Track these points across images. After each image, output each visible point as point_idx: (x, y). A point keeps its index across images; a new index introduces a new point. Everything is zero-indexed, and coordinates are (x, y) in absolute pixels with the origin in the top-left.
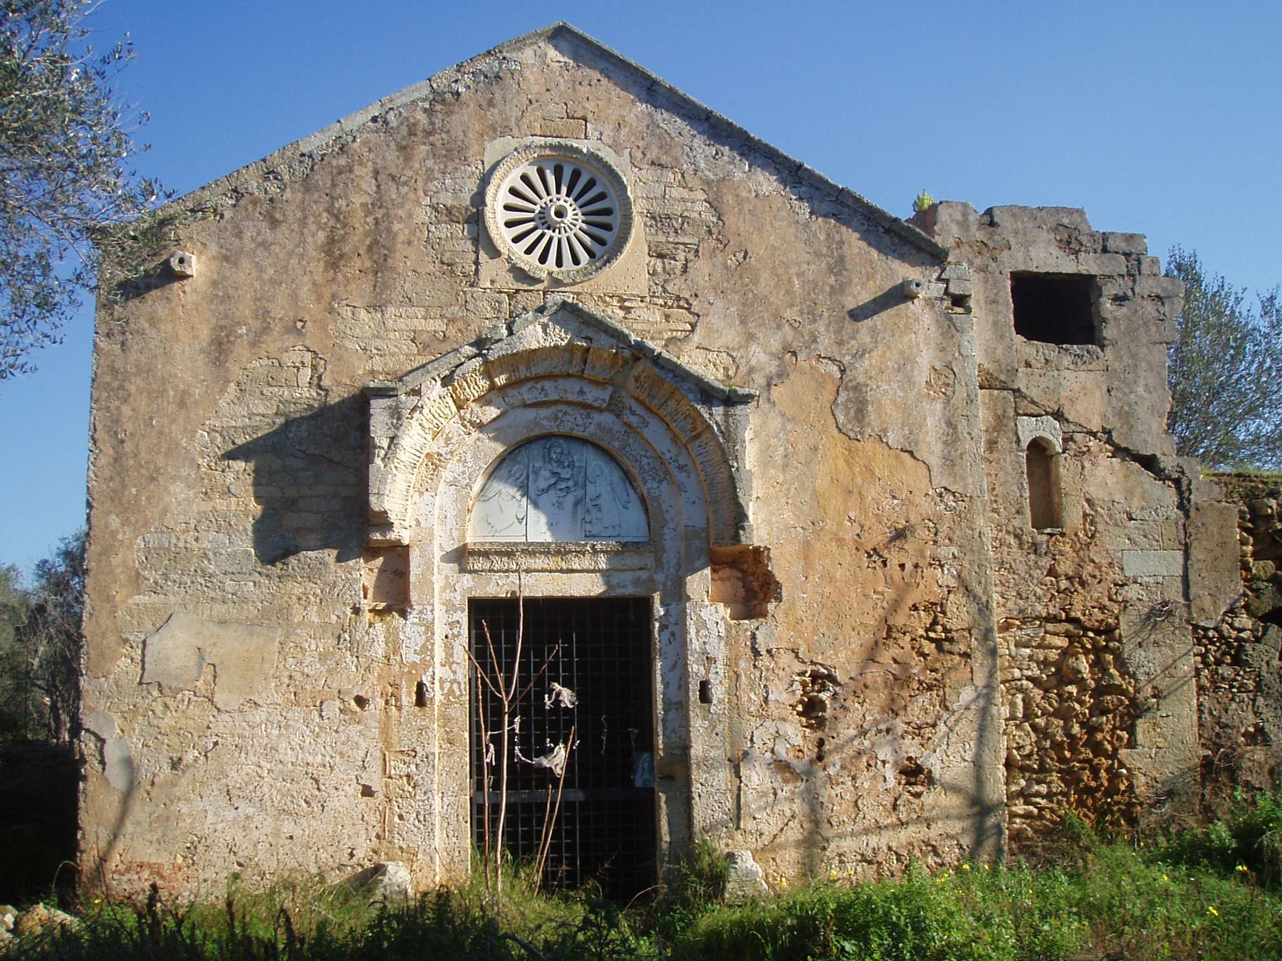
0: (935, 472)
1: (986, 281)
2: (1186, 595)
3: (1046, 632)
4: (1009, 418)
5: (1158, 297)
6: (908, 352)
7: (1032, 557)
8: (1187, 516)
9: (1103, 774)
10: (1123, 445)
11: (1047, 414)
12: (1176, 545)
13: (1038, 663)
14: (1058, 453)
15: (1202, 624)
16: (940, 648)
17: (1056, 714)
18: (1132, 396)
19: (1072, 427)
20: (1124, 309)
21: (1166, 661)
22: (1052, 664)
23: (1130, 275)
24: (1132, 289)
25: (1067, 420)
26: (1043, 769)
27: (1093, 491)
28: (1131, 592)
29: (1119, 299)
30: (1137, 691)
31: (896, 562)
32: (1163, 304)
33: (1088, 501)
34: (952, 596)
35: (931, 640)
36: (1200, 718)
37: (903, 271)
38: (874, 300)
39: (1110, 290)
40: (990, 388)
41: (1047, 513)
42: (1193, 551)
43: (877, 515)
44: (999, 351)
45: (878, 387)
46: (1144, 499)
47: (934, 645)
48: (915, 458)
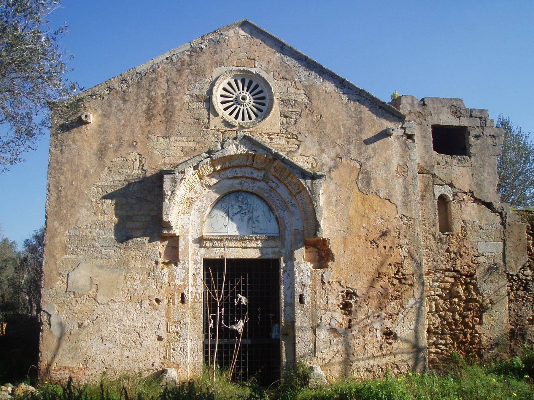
0: (399, 208)
1: (421, 129)
2: (504, 261)
5: (493, 136)
7: (440, 244)
8: (505, 228)
9: (468, 336)
11: (446, 184)
12: (500, 240)
13: (442, 289)
15: (511, 273)
17: (449, 310)
18: (482, 177)
19: (457, 190)
20: (479, 141)
22: (448, 289)
23: (482, 127)
24: (483, 133)
25: (455, 187)
26: (443, 333)
27: (465, 217)
28: (481, 259)
29: (477, 137)
30: (483, 301)
33: (463, 221)
34: (406, 260)
36: (509, 313)
37: (387, 124)
38: (375, 136)
39: (473, 133)
40: (422, 173)
41: (446, 226)
43: (374, 226)
44: (426, 158)
45: (376, 172)
46: (486, 220)
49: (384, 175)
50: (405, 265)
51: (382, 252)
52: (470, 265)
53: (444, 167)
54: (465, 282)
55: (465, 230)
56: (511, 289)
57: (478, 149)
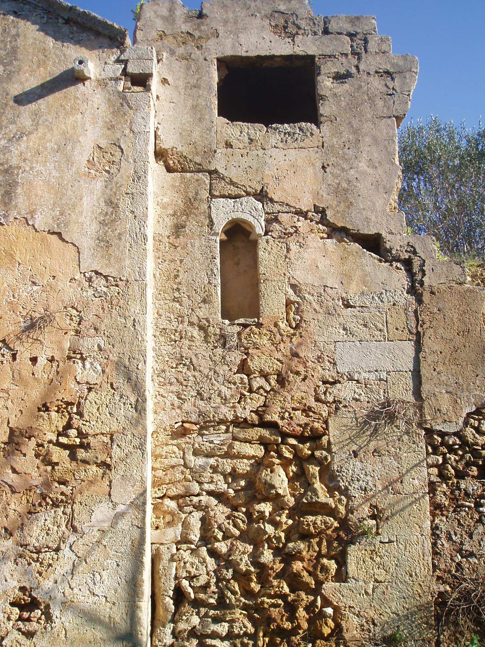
0: (86, 254)
1: (188, 68)
2: (417, 393)
3: (235, 439)
4: (201, 200)
5: (387, 73)
6: (71, 132)
7: (219, 351)
8: (420, 301)
9: (301, 613)
10: (340, 224)
11: (248, 194)
12: (406, 334)
13: (225, 476)
14: (260, 236)
15: (438, 428)
16: (73, 457)
17: (244, 537)
18: (352, 172)
19: (277, 207)
20: (346, 86)
21: (389, 475)
22: (243, 476)
23: (354, 53)
24: (357, 67)
25: (272, 200)
26: (222, 604)
27: (300, 275)
28: (345, 391)
29: (340, 77)
30: (350, 510)
31: (28, 355)
32: (393, 79)
33: (294, 287)
34: (92, 394)
35: (64, 446)
36: (434, 544)
37: (71, 54)
38: (42, 85)
39: (328, 69)
40: (183, 170)
41: (242, 299)
42: (426, 341)
43: (11, 303)
44: (196, 135)
45: (32, 168)
46: (365, 283)
47: (68, 452)
48: (63, 240)
49: (55, 173)
50: (88, 408)
51: (24, 372)
52: (310, 409)
53: (244, 152)
54: (295, 455)
55: (298, 311)
56: (441, 475)
57: (343, 104)
